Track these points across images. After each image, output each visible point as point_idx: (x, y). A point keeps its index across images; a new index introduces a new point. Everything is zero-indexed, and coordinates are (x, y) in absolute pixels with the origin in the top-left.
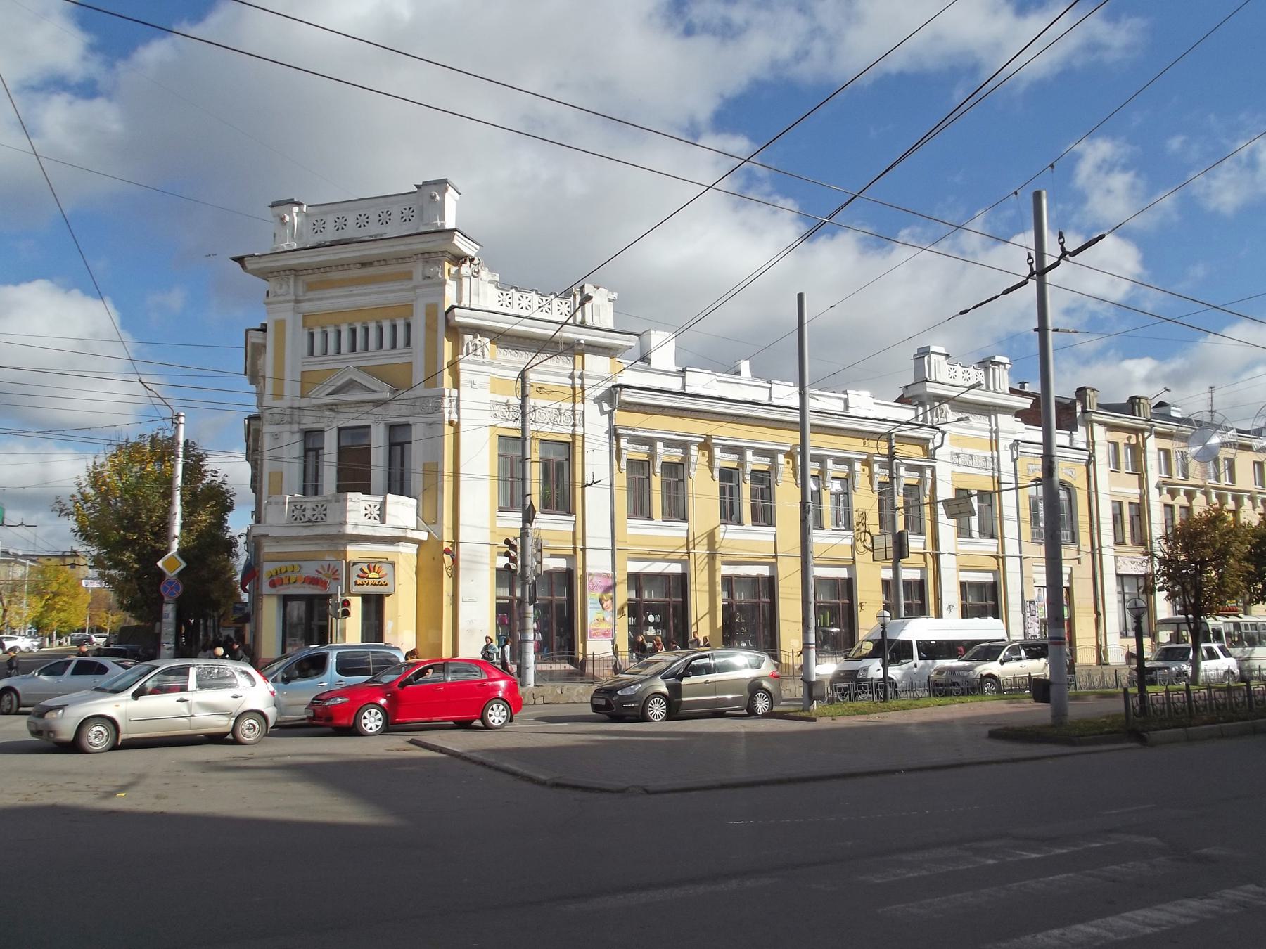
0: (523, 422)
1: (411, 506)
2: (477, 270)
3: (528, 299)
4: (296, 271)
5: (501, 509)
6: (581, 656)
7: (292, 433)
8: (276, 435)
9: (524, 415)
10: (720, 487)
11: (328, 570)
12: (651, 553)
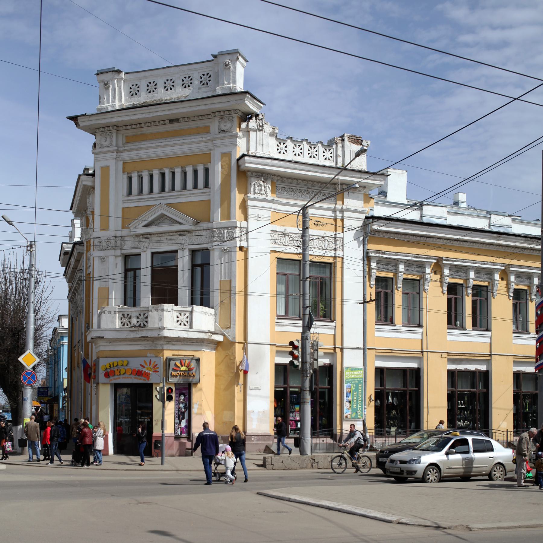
0: (304, 249)
1: (211, 314)
2: (261, 125)
3: (300, 147)
4: (117, 127)
5: (279, 317)
6: (339, 431)
7: (116, 257)
8: (103, 258)
9: (304, 243)
10: (448, 299)
11: (150, 365)
12: (393, 351)
